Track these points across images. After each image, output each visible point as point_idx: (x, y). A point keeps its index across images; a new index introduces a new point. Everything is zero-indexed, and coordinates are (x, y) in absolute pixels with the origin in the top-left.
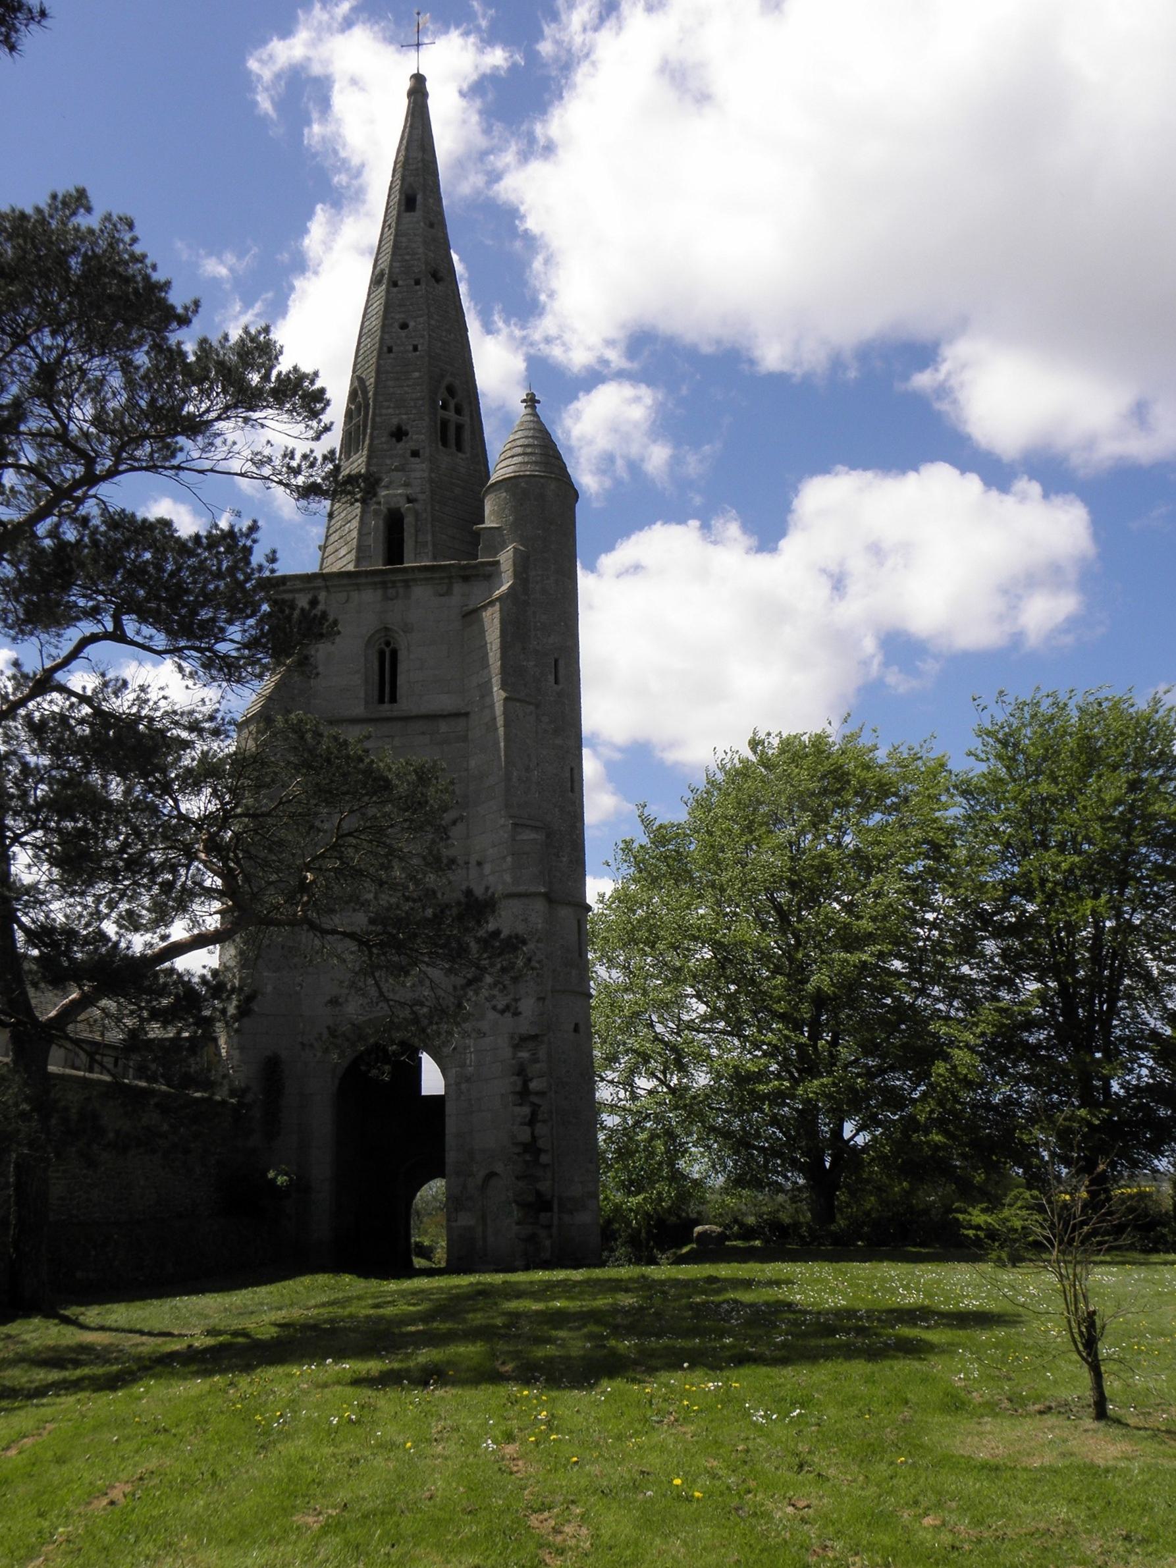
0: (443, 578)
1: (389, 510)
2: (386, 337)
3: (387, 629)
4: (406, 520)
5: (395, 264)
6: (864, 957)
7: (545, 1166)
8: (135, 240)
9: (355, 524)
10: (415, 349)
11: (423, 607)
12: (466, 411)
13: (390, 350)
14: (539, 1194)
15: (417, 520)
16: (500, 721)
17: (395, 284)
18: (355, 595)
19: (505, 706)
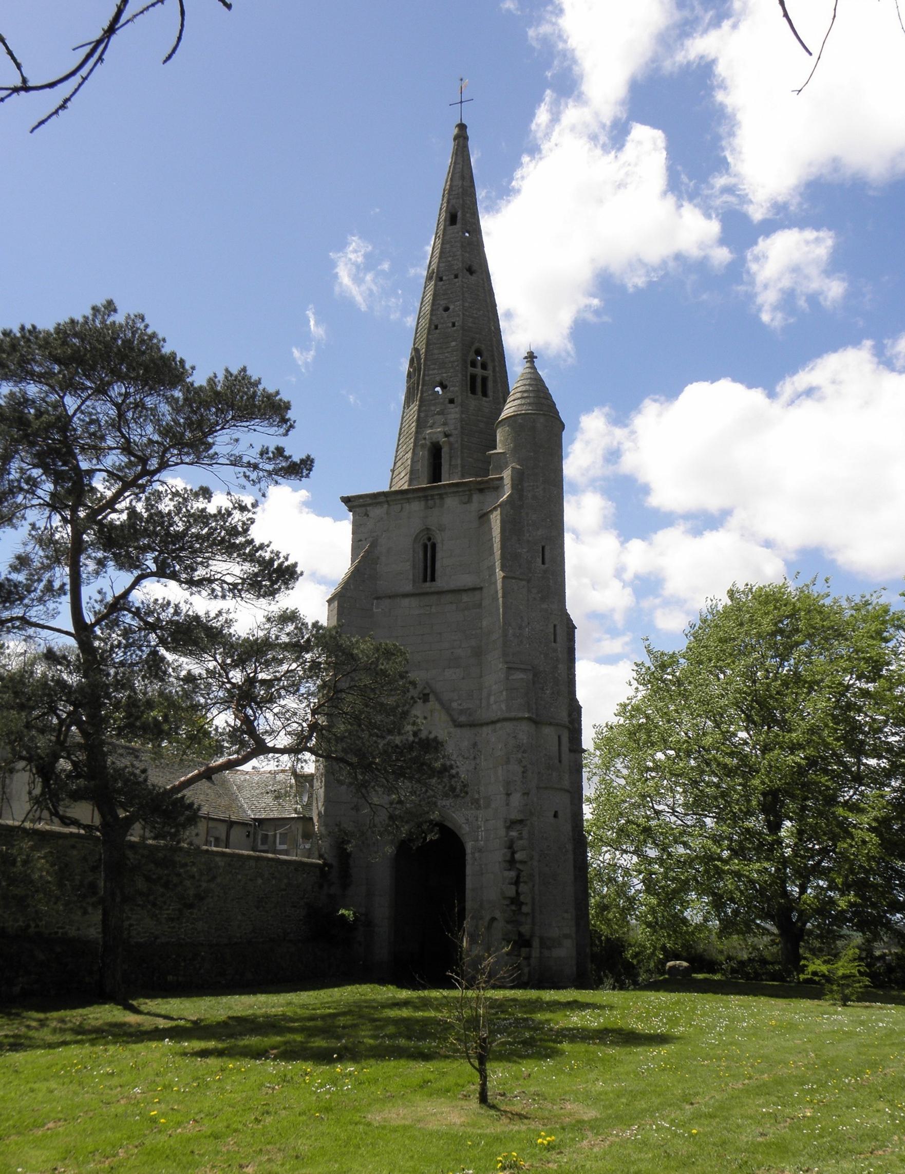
0: (464, 491)
1: (432, 443)
2: (434, 318)
3: (428, 529)
4: (443, 450)
5: (441, 265)
6: (797, 759)
7: (527, 914)
8: (147, 326)
9: (409, 455)
10: (454, 325)
11: (452, 514)
12: (490, 367)
13: (436, 327)
14: (520, 934)
15: (451, 449)
16: (500, 594)
17: (441, 279)
18: (407, 506)
19: (503, 582)
